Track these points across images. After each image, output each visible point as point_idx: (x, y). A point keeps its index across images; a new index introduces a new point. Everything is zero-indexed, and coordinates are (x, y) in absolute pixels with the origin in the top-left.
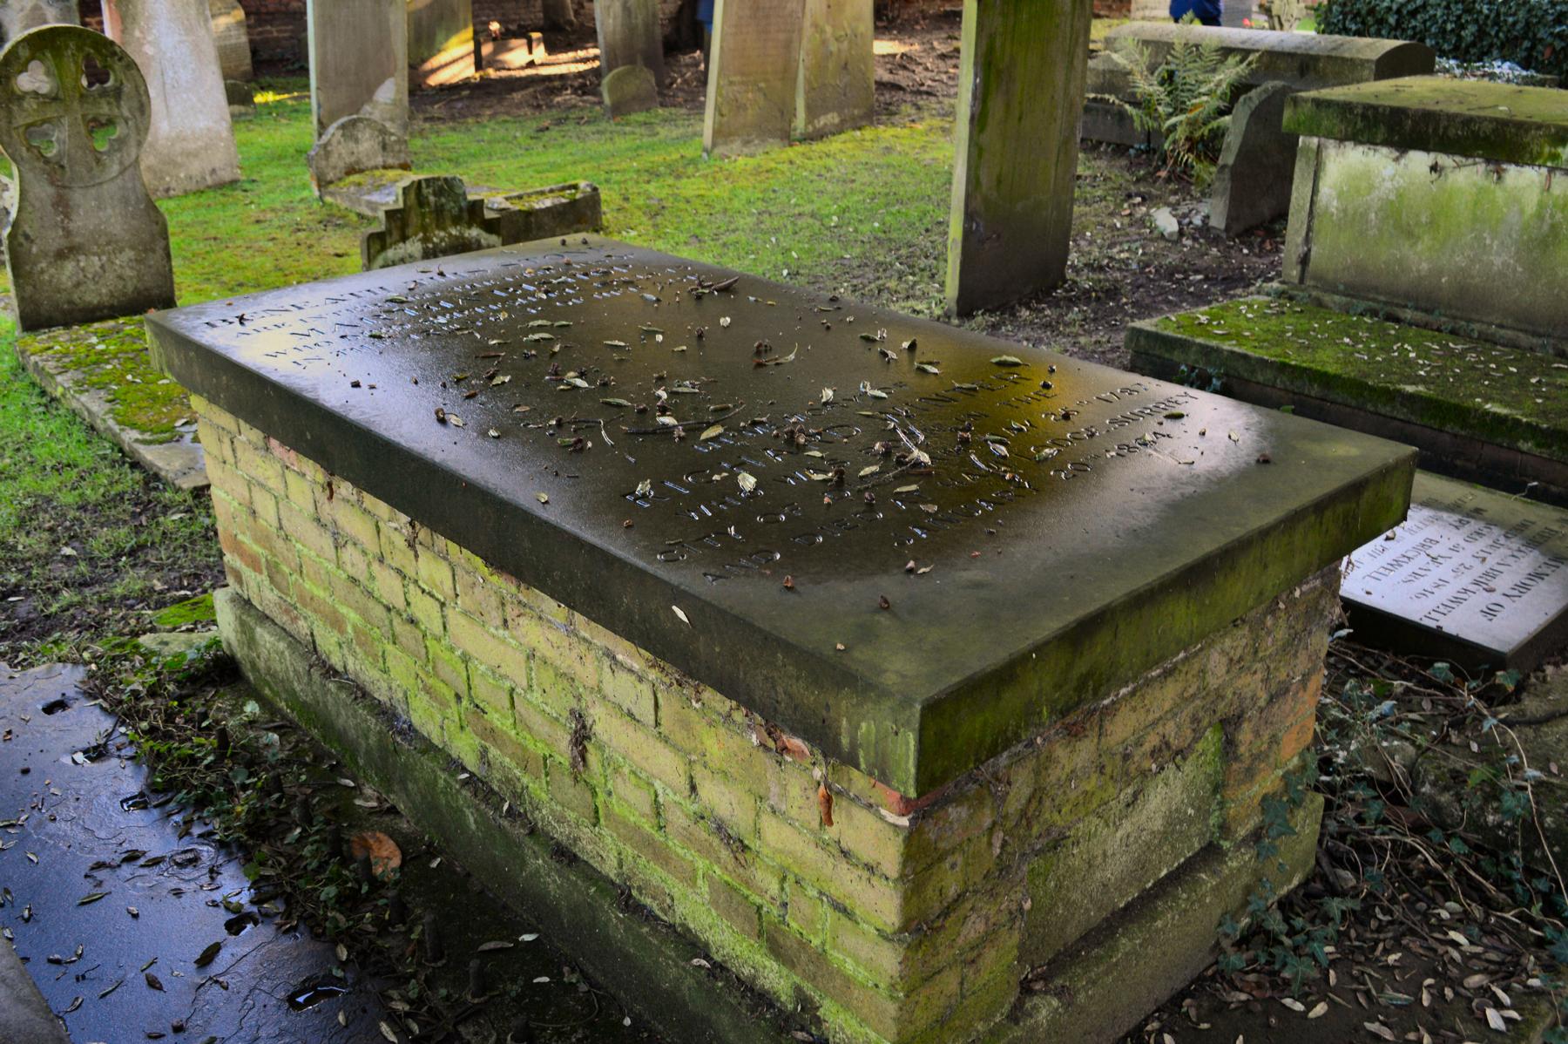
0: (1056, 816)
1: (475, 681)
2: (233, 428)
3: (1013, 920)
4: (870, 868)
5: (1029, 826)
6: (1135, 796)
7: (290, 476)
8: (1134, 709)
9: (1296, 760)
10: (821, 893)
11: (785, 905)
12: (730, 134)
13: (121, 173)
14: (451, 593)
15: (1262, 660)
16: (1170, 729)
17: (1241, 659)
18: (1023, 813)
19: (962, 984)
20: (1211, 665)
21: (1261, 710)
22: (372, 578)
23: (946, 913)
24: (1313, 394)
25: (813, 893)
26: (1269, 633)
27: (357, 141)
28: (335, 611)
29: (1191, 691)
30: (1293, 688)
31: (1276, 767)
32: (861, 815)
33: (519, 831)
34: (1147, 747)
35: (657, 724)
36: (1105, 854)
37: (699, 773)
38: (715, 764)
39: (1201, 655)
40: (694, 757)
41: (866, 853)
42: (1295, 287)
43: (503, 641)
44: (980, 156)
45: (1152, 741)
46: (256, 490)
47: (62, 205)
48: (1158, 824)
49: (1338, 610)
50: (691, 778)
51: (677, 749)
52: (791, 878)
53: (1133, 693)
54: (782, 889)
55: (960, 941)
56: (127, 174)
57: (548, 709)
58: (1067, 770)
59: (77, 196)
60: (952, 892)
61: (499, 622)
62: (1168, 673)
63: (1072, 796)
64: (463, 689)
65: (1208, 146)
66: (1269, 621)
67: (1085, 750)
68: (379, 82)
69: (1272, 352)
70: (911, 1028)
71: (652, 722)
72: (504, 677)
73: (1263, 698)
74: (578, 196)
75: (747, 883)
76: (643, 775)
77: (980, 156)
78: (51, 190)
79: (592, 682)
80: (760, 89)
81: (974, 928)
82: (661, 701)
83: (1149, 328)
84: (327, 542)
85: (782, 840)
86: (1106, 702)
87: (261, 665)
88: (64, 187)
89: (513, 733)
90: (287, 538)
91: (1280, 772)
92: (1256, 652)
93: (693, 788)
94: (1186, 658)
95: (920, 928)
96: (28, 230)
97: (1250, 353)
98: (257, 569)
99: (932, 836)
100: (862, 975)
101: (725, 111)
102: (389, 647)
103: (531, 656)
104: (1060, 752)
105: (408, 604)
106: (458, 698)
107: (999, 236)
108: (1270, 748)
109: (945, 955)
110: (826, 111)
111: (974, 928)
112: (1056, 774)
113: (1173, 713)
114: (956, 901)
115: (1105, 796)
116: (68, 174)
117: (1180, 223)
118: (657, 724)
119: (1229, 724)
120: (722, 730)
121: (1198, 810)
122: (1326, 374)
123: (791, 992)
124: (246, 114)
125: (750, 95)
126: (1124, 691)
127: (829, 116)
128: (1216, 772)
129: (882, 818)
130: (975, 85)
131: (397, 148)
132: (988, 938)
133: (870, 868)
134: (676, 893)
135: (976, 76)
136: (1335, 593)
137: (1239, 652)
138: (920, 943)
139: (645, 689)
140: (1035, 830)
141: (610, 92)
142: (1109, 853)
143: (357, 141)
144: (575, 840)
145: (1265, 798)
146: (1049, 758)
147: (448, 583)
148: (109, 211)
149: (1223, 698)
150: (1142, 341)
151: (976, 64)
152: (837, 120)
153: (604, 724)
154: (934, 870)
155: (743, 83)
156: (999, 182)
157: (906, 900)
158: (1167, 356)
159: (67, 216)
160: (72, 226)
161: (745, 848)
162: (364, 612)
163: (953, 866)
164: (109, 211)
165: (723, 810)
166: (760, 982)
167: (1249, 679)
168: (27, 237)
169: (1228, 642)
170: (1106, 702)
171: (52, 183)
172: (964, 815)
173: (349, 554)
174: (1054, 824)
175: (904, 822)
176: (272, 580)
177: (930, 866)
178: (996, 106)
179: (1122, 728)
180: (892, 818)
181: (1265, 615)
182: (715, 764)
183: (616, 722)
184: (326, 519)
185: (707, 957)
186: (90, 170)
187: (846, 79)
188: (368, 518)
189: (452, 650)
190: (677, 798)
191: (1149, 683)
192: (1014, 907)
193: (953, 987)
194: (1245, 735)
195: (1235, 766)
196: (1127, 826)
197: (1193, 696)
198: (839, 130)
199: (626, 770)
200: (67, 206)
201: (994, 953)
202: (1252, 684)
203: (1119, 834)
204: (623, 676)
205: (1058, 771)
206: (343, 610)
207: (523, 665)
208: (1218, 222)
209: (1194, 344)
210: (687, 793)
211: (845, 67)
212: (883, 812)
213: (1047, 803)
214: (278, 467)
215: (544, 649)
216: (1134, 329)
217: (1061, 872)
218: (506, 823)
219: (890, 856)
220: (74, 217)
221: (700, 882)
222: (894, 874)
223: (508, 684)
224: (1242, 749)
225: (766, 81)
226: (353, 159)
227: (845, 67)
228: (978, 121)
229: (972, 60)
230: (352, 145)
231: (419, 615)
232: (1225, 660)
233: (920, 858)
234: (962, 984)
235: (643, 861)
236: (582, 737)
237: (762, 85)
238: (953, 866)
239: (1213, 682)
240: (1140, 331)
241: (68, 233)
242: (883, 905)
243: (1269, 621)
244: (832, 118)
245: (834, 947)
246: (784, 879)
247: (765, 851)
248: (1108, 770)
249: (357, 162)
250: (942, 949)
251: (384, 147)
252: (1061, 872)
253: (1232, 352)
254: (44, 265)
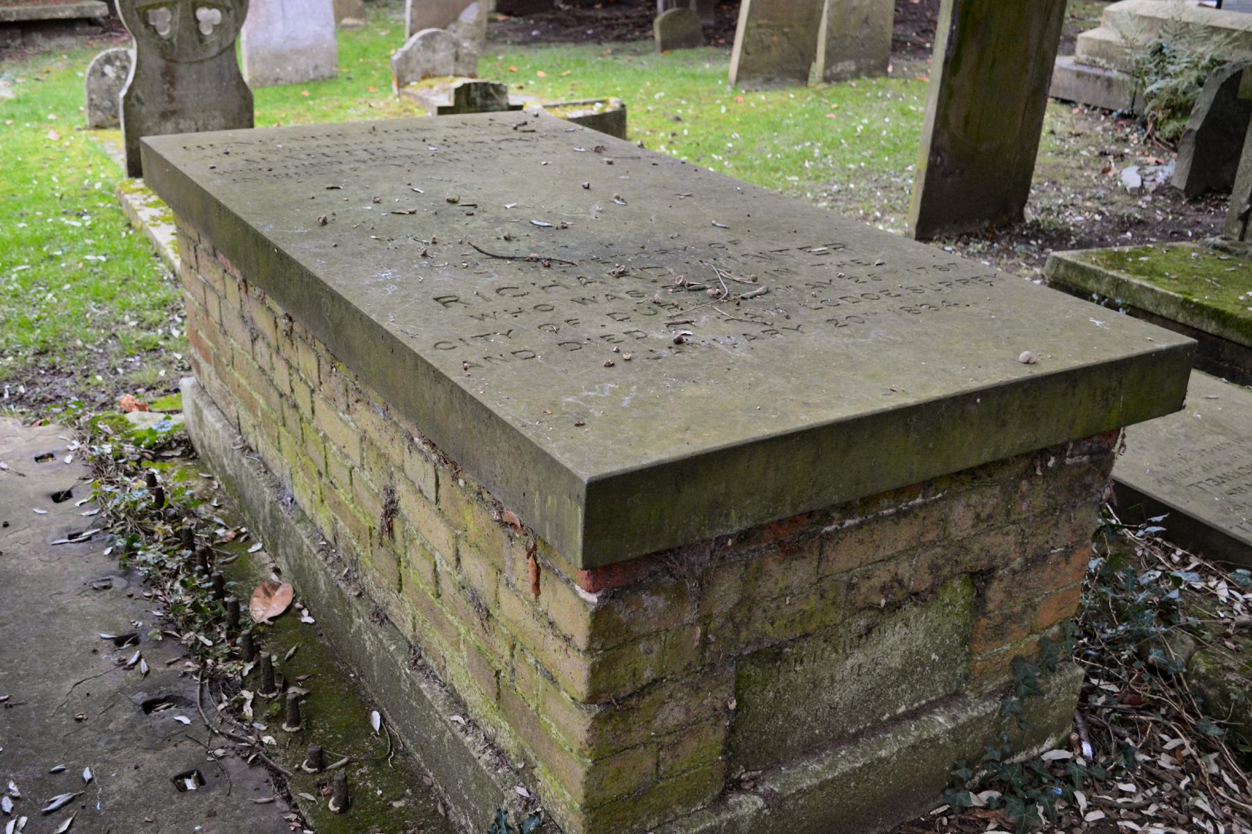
0: (768, 628)
1: (330, 460)
2: (195, 237)
3: (718, 718)
4: (567, 640)
5: (737, 630)
6: (869, 630)
7: (227, 277)
8: (861, 542)
9: (1055, 629)
10: (537, 662)
11: (513, 670)
12: (754, 71)
13: (220, 53)
14: (317, 380)
15: (1014, 523)
16: (904, 569)
17: (990, 516)
18: (731, 617)
19: (658, 765)
20: (955, 516)
21: (1014, 572)
22: (273, 369)
23: (641, 692)
24: (1210, 330)
25: (531, 660)
26: (1023, 498)
27: (434, 51)
28: (251, 398)
29: (931, 536)
30: (1053, 558)
31: (1032, 632)
32: (561, 588)
33: (351, 593)
34: (876, 582)
35: (437, 500)
36: (833, 680)
37: (463, 548)
38: (472, 539)
39: (942, 504)
40: (459, 532)
41: (566, 626)
42: (1236, 245)
43: (346, 424)
44: (950, 96)
45: (882, 576)
46: (208, 290)
47: (169, 76)
48: (896, 662)
49: (1108, 491)
50: (458, 551)
51: (448, 523)
52: (518, 647)
53: (859, 526)
54: (512, 656)
55: (657, 723)
56: (224, 55)
57: (373, 486)
58: (781, 585)
59: (182, 70)
60: (648, 675)
61: (344, 407)
62: (900, 515)
63: (787, 611)
64: (322, 466)
65: (1178, 108)
66: (1024, 485)
67: (801, 572)
68: (465, 5)
69: (1178, 289)
70: (600, 795)
71: (434, 499)
72: (347, 456)
73: (1017, 563)
74: (608, 110)
75: (491, 648)
76: (428, 547)
77: (950, 96)
78: (161, 62)
79: (398, 462)
80: (785, 34)
81: (672, 715)
82: (440, 481)
83: (1069, 259)
84: (246, 337)
85: (513, 609)
86: (828, 529)
87: (206, 443)
88: (172, 61)
89: (352, 506)
90: (225, 333)
91: (1037, 638)
92: (1008, 514)
93: (458, 560)
94: (925, 504)
95: (613, 702)
96: (140, 95)
97: (1157, 288)
98: (208, 361)
99: (623, 617)
100: (562, 739)
101: (750, 50)
102: (282, 429)
103: (363, 439)
104: (774, 567)
105: (293, 391)
106: (320, 474)
107: (962, 172)
108: (1024, 612)
109: (638, 735)
110: (843, 59)
111: (672, 715)
112: (767, 587)
113: (910, 552)
114: (648, 685)
115: (827, 620)
116: (176, 50)
117: (1143, 181)
118: (437, 500)
119: (980, 578)
120: (476, 507)
121: (943, 656)
122: (1223, 312)
123: (516, 751)
124: (358, 26)
125: (775, 39)
126: (849, 522)
127: (847, 63)
128: (966, 625)
129: (575, 593)
130: (952, 32)
131: (467, 59)
132: (689, 728)
133: (567, 640)
134: (447, 655)
135: (953, 22)
136: (1105, 474)
137: (988, 510)
138: (611, 716)
139: (429, 467)
140: (744, 635)
141: (662, 27)
142: (838, 677)
143: (434, 51)
144: (388, 604)
145: (1016, 659)
146: (760, 569)
147: (315, 373)
148: (207, 84)
149: (968, 551)
150: (1062, 269)
151: (954, 12)
152: (853, 68)
153: (407, 502)
154: (626, 651)
155: (769, 27)
156: (967, 123)
157: (594, 672)
158: (1082, 284)
159: (172, 84)
160: (176, 94)
161: (489, 615)
162: (267, 399)
163: (649, 652)
164: (207, 84)
165: (476, 582)
166: (498, 740)
167: (999, 539)
168: (138, 99)
169: (974, 498)
170: (828, 529)
171: (163, 57)
172: (660, 606)
173: (260, 346)
174: (765, 634)
175: (593, 598)
176: (217, 372)
177: (619, 647)
178: (970, 56)
179: (846, 557)
180: (584, 594)
181: (1020, 478)
182: (472, 539)
183: (413, 498)
184: (247, 315)
185: (464, 715)
186: (194, 49)
187: (866, 31)
188: (270, 314)
189: (317, 431)
190: (449, 569)
191: (879, 519)
192: (719, 705)
193: (648, 763)
194: (995, 592)
195: (984, 621)
196: (858, 657)
197: (933, 544)
198: (856, 75)
199: (418, 542)
200: (173, 76)
201: (695, 744)
202: (1003, 545)
203: (850, 662)
204: (416, 455)
205: (770, 585)
206: (257, 396)
207: (358, 445)
208: (1180, 183)
209: (1107, 275)
210: (454, 563)
211: (866, 21)
212: (577, 588)
213: (758, 613)
214: (221, 271)
215: (373, 434)
216: (1055, 257)
217: (780, 685)
218: (342, 585)
219: (579, 629)
220: (178, 86)
221: (462, 646)
222: (583, 647)
223: (349, 464)
224: (991, 606)
225: (791, 26)
226: (429, 66)
227: (866, 21)
228: (952, 64)
229: (950, 10)
230: (430, 54)
231: (299, 401)
232: (971, 514)
233: (608, 636)
234: (658, 765)
235: (427, 625)
236: (391, 511)
237: (786, 30)
238: (649, 652)
239: (955, 533)
240: (1060, 260)
241: (172, 99)
242: (575, 672)
243: (1024, 485)
244: (850, 66)
245: (544, 712)
246: (514, 647)
247: (502, 620)
248: (831, 595)
249: (434, 69)
250: (635, 727)
251: (457, 58)
252: (780, 685)
253: (1141, 286)
254: (150, 124)
